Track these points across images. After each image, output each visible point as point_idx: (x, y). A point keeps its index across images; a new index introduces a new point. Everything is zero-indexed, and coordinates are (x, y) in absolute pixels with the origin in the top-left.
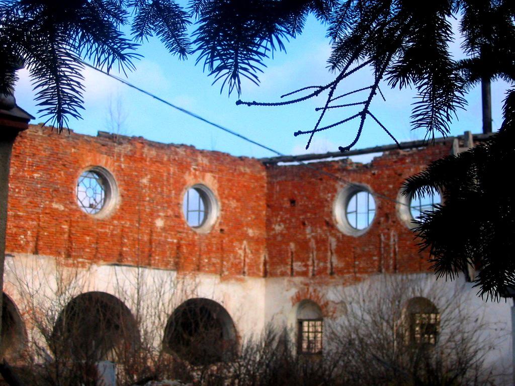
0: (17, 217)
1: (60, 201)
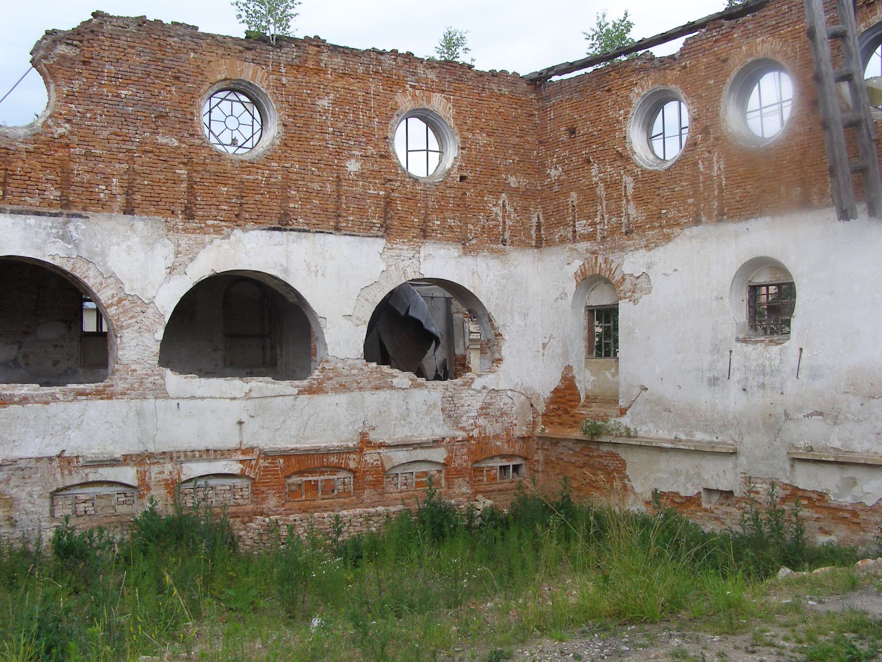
1: (171, 132)
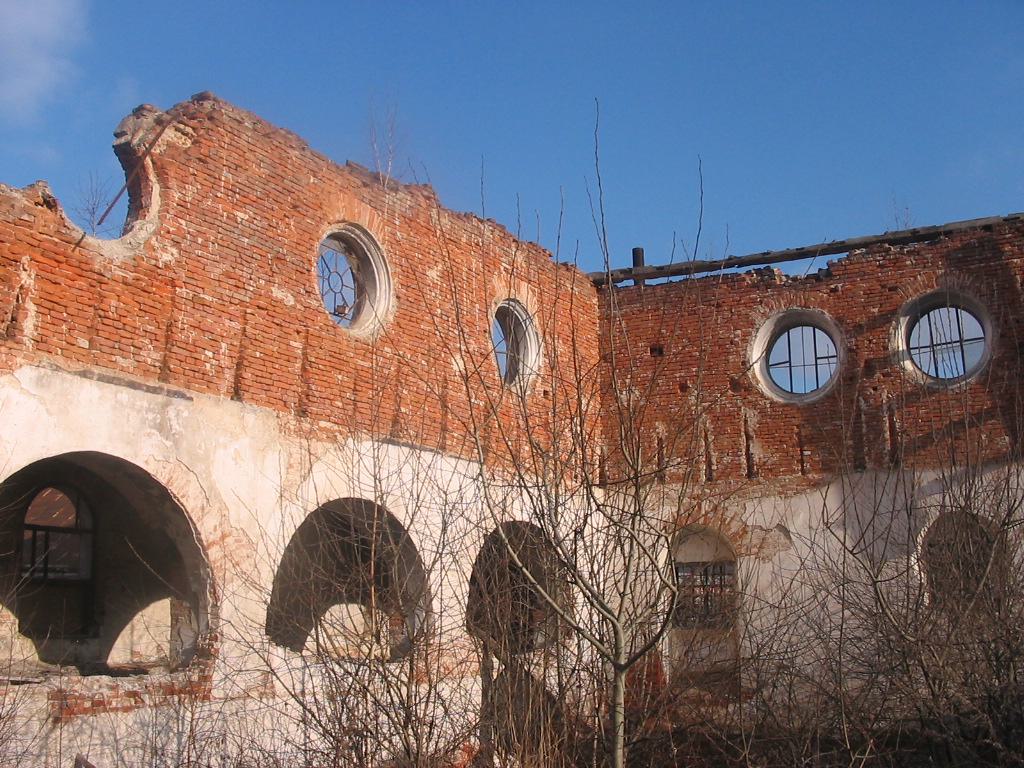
0: (197, 303)
